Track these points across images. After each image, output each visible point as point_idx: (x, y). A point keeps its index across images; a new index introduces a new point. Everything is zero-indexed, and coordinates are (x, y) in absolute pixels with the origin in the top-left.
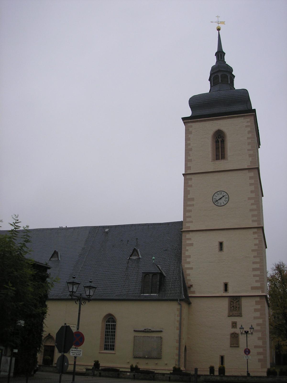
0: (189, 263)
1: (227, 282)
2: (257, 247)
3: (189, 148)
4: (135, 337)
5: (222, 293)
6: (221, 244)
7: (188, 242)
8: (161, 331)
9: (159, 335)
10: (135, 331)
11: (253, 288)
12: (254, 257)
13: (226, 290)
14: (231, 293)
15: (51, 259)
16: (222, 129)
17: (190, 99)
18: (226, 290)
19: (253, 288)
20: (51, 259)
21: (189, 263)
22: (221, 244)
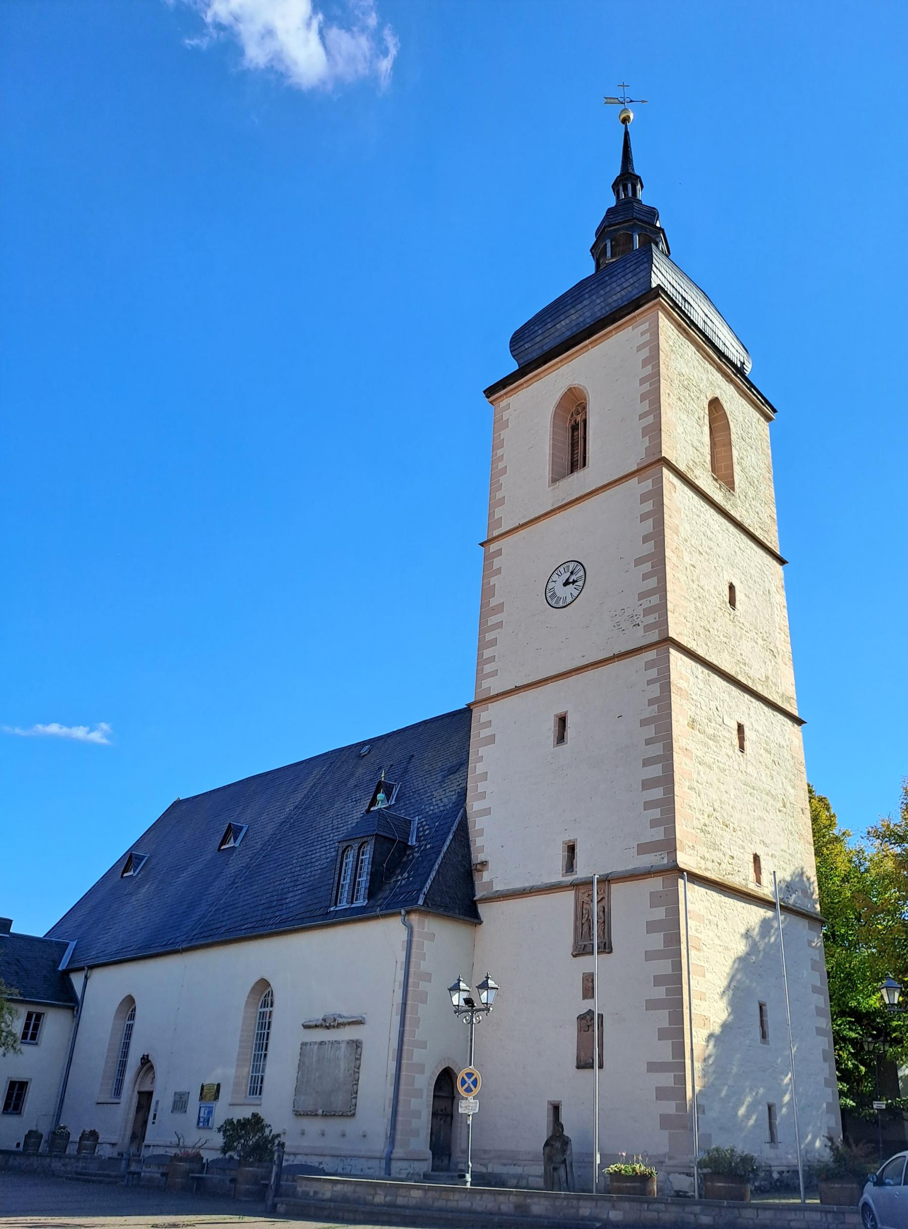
0: (483, 796)
1: (572, 838)
2: (663, 989)
3: (672, 1074)
4: (304, 1044)
5: (557, 876)
6: (562, 721)
7: (484, 733)
8: (359, 1022)
9: (346, 1034)
10: (306, 1027)
11: (643, 849)
12: (648, 742)
13: (570, 867)
14: (582, 871)
15: (223, 847)
16: (579, 381)
17: (511, 343)
18: (570, 867)
19: (643, 849)
20: (223, 847)
21: (483, 796)
22: (562, 721)
